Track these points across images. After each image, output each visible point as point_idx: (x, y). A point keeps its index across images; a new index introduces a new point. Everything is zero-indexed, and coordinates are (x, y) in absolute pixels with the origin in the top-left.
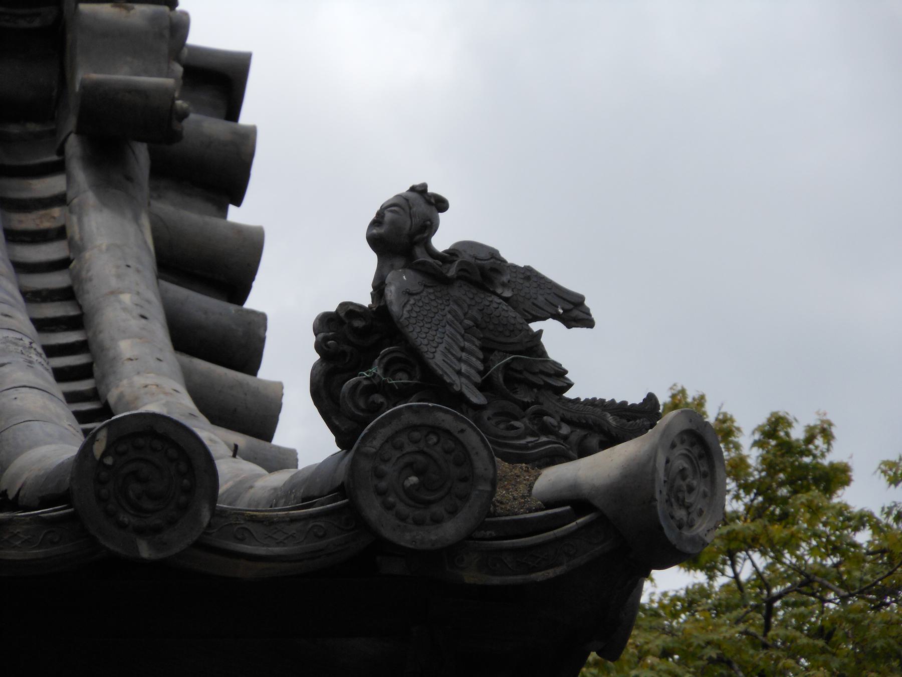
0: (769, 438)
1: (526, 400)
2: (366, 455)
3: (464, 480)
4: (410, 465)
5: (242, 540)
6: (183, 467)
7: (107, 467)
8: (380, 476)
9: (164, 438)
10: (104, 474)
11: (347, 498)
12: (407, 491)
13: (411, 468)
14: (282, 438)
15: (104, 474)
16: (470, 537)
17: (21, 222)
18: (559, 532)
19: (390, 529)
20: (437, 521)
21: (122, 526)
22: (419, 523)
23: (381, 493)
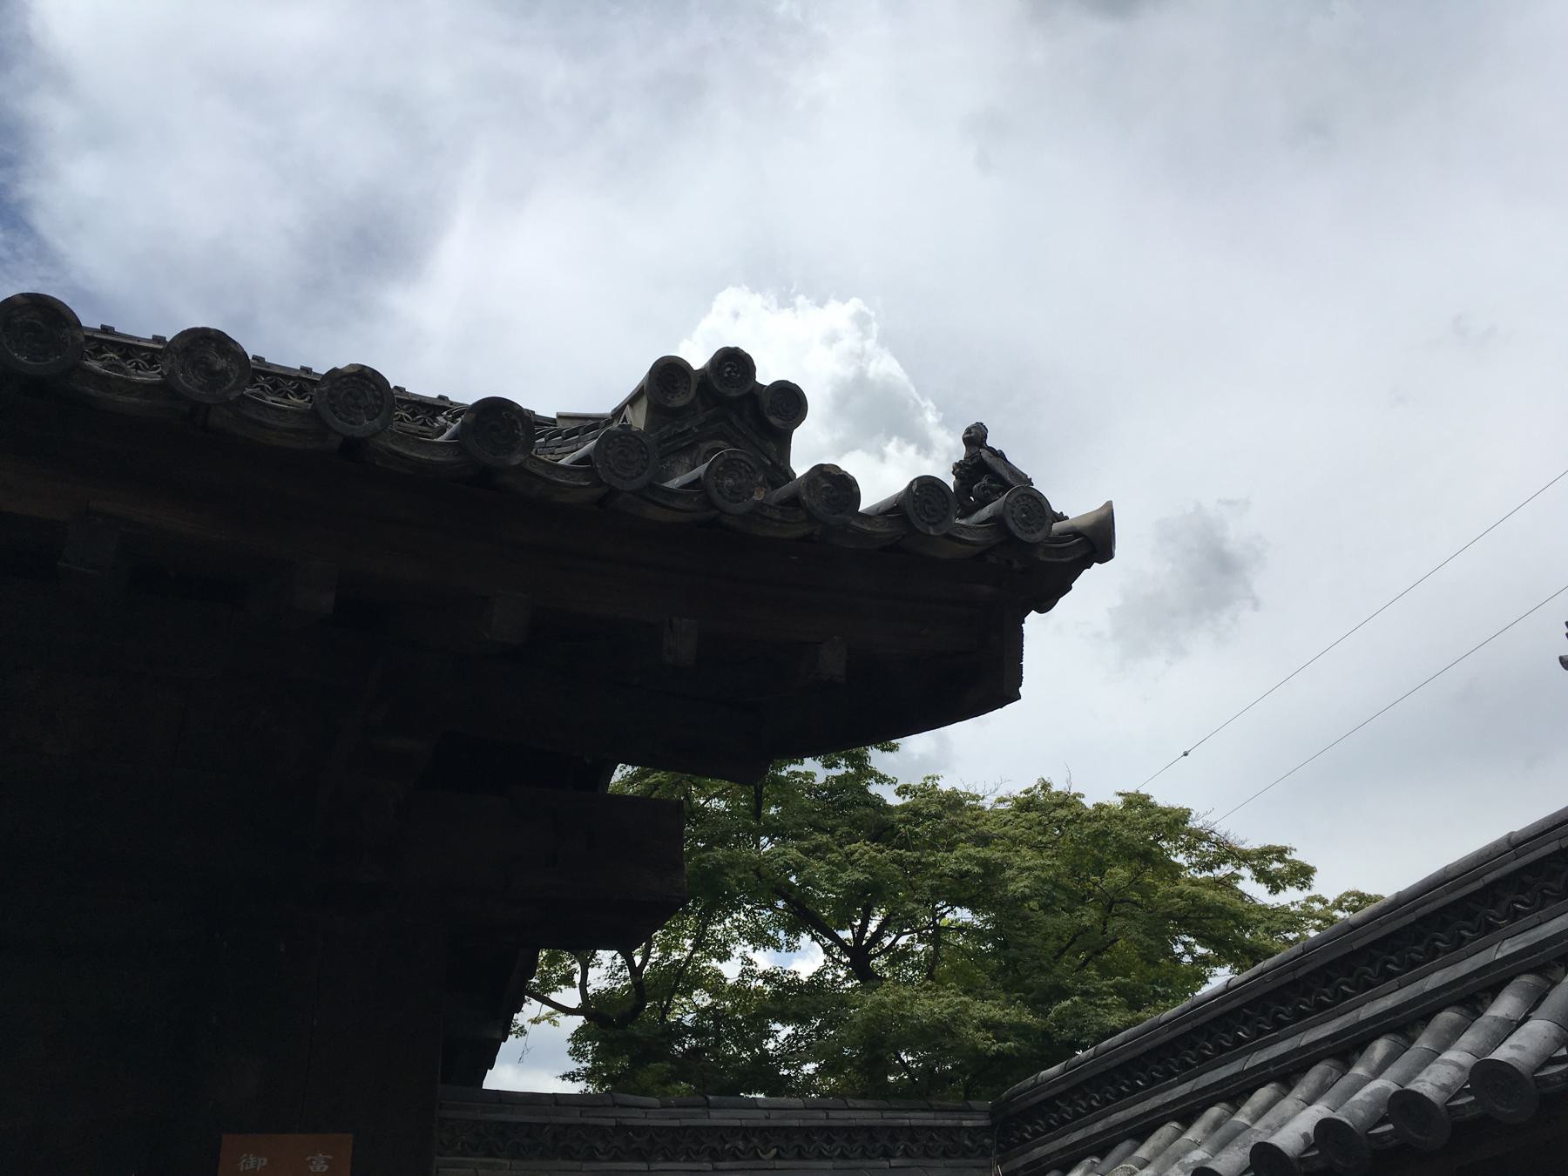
0: (972, 491)
1: (604, 480)
2: (1009, 504)
3: (1041, 517)
4: (1023, 509)
5: (960, 534)
6: (944, 500)
7: (916, 496)
8: (1013, 512)
9: (940, 489)
10: (916, 499)
11: (1390, 1123)
12: (1023, 519)
13: (1024, 511)
14: (1275, 862)
15: (916, 499)
16: (1042, 542)
17: (1459, 1056)
18: (1070, 543)
19: (1019, 534)
20: (1033, 532)
21: (923, 520)
22: (1027, 532)
23: (1013, 519)
